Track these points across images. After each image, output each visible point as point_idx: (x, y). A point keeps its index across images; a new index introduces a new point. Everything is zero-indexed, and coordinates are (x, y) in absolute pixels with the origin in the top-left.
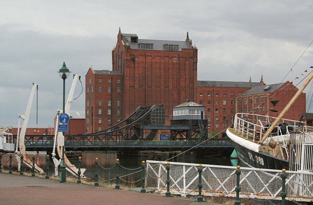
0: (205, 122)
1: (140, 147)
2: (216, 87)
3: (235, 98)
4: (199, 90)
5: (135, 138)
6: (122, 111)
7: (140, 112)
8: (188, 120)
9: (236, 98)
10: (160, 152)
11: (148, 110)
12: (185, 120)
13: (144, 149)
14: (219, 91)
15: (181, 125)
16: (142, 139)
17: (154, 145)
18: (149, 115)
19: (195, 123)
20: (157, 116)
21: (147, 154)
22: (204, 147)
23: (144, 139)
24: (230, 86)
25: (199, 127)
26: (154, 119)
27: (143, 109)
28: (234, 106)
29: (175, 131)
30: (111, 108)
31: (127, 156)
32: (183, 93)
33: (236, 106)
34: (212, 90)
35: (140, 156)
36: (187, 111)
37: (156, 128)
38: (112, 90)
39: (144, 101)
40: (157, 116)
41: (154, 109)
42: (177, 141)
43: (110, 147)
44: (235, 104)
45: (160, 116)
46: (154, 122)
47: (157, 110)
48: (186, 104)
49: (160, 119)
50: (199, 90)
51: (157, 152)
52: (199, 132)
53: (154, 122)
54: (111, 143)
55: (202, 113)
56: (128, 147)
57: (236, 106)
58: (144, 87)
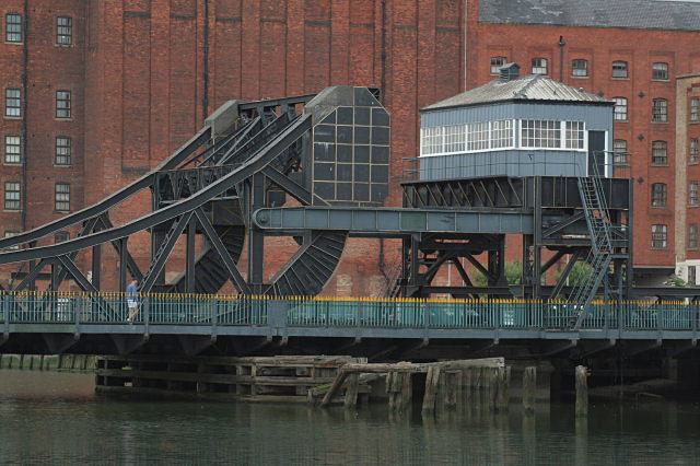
0: (617, 194)
1: (245, 331)
2: (577, 27)
3: (672, 87)
4: (491, 38)
5: (208, 275)
6: (78, 147)
7: (231, 131)
8: (515, 180)
9: (681, 86)
10: (363, 363)
11: (283, 122)
12: (503, 179)
13: (273, 347)
14: (591, 51)
15: (468, 208)
16: (254, 286)
17: (328, 323)
18: (292, 156)
19: (561, 197)
20: (344, 153)
21: (290, 372)
22: (613, 336)
23: (268, 289)
24: (645, 24)
25: (583, 223)
26: (323, 171)
27: (250, 113)
28: (670, 128)
29: (429, 241)
30: (23, 127)
31: (161, 384)
32: (404, 58)
33: (681, 127)
34: (553, 39)
35: (247, 388)
36: (515, 127)
37: (339, 223)
38: (26, 35)
39: (200, 93)
40: (344, 153)
41: (325, 113)
42: (437, 299)
43: (71, 329)
44: (672, 115)
45: (362, 154)
46: (325, 191)
47: (345, 115)
48: (503, 90)
49: (361, 172)
50: (491, 38)
51: (352, 363)
52: (582, 251)
53: (325, 191)
54: (67, 307)
55: (596, 139)
56: (176, 330)
57: (681, 127)
58: (200, 20)
